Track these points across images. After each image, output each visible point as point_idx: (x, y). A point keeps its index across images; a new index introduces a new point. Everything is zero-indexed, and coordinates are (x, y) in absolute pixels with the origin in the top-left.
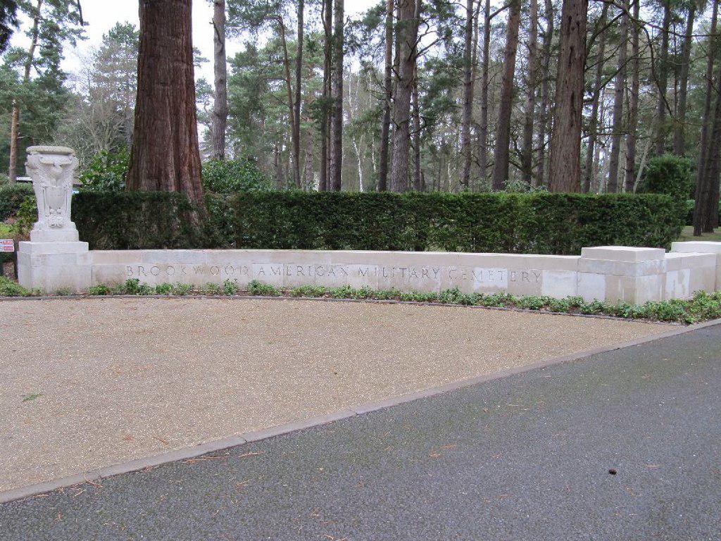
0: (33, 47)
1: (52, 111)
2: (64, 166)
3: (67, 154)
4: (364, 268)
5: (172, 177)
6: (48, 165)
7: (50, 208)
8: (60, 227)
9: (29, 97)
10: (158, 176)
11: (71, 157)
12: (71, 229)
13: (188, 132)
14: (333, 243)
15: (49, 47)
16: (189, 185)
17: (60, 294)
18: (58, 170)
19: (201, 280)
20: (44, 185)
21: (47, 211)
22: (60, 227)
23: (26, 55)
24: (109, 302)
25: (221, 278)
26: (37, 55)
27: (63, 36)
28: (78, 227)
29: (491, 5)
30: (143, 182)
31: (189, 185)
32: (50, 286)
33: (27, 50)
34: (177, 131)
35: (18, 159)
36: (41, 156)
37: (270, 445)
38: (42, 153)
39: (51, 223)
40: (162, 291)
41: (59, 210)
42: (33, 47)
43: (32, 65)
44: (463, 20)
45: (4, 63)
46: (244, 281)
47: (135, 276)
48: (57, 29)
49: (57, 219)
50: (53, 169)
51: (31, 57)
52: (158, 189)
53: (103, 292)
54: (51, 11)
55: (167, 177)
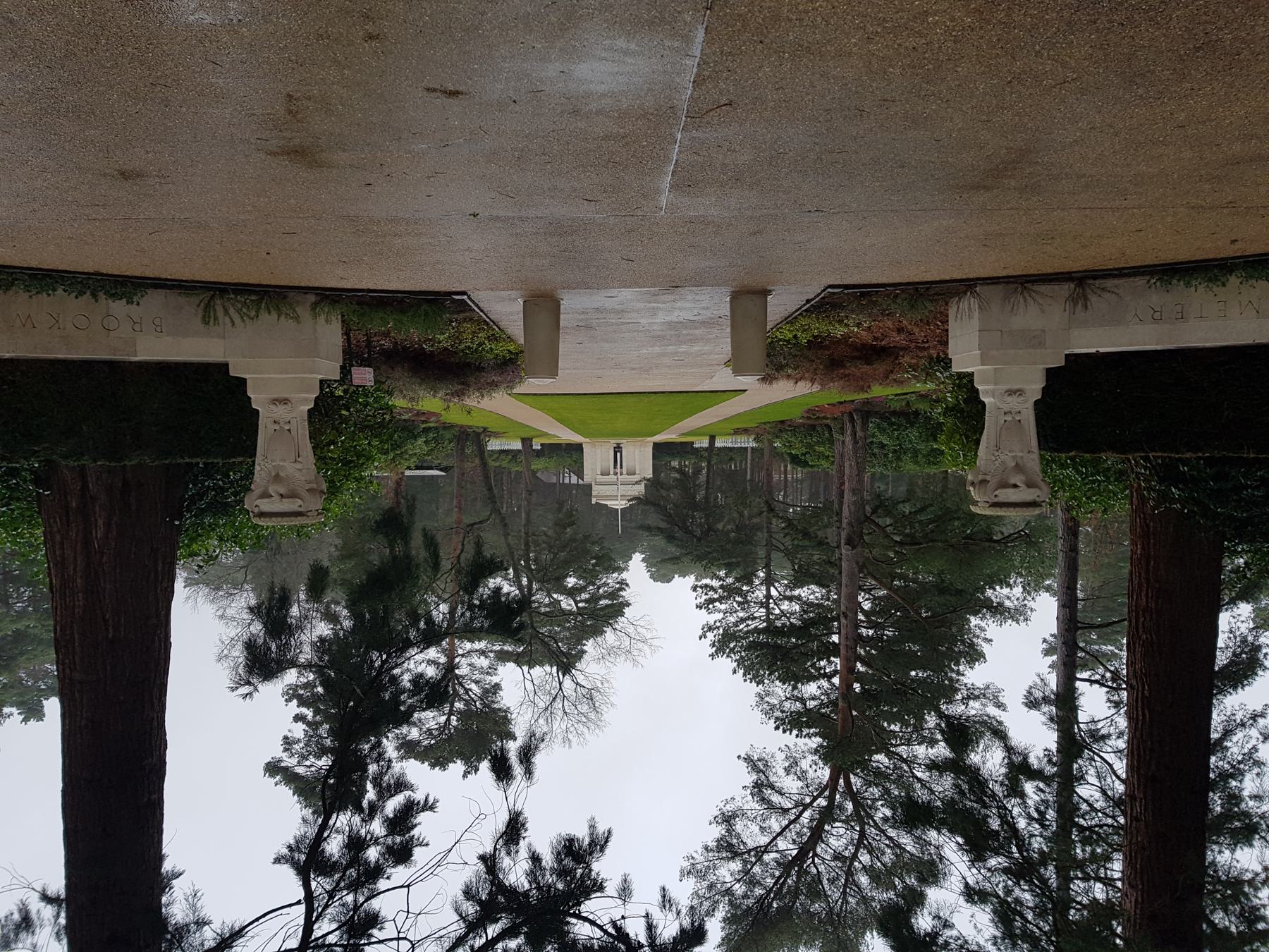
2: (266, 495)
3: (262, 515)
6: (293, 495)
7: (289, 430)
8: (275, 401)
11: (256, 510)
12: (257, 398)
20: (299, 466)
21: (293, 427)
22: (275, 401)
29: (1087, 677)
35: (190, 924)
36: (301, 510)
38: (300, 514)
39: (288, 407)
41: (277, 427)
43: (1100, 733)
44: (299, 741)
45: (450, 765)
49: (280, 411)
50: (282, 491)
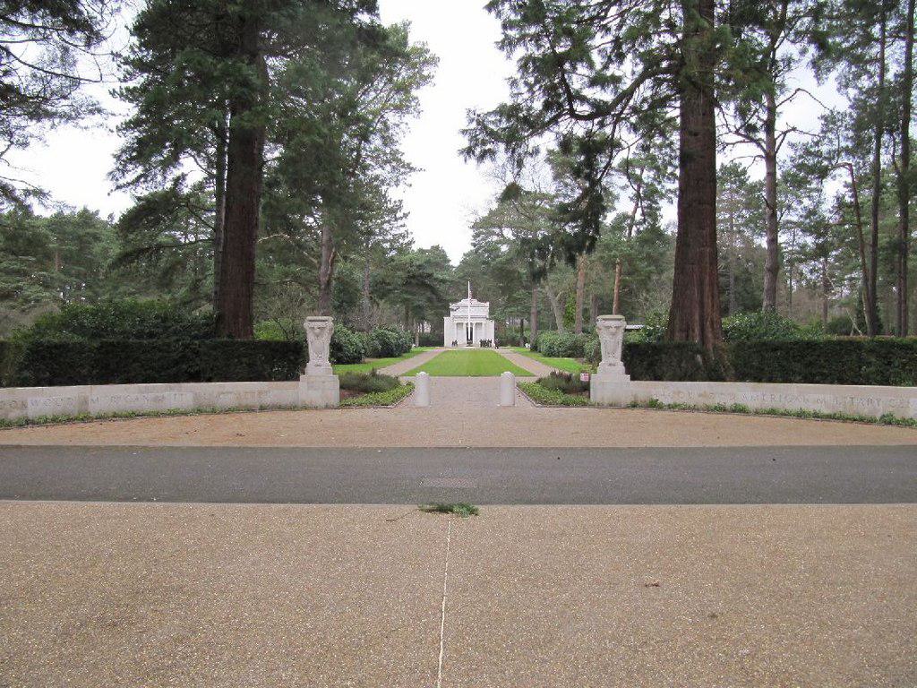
0: (635, 211)
1: (649, 265)
4: (821, 397)
5: (697, 331)
6: (608, 327)
9: (630, 255)
10: (687, 330)
12: (621, 366)
13: (710, 298)
14: (809, 379)
15: (650, 207)
16: (710, 335)
17: (611, 405)
18: (613, 330)
19: (701, 402)
23: (628, 217)
24: (636, 411)
25: (717, 400)
26: (638, 217)
27: (662, 196)
28: (625, 365)
30: (677, 334)
31: (710, 335)
32: (606, 402)
33: (630, 213)
34: (702, 297)
37: (72, 385)
40: (671, 407)
42: (635, 211)
46: (729, 403)
47: (655, 398)
48: (656, 191)
49: (612, 360)
51: (633, 218)
52: (687, 340)
53: (634, 406)
54: (653, 176)
55: (693, 331)
